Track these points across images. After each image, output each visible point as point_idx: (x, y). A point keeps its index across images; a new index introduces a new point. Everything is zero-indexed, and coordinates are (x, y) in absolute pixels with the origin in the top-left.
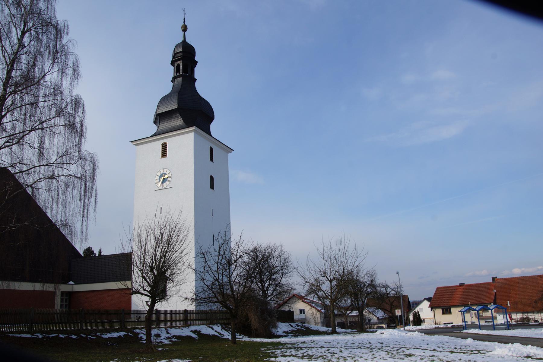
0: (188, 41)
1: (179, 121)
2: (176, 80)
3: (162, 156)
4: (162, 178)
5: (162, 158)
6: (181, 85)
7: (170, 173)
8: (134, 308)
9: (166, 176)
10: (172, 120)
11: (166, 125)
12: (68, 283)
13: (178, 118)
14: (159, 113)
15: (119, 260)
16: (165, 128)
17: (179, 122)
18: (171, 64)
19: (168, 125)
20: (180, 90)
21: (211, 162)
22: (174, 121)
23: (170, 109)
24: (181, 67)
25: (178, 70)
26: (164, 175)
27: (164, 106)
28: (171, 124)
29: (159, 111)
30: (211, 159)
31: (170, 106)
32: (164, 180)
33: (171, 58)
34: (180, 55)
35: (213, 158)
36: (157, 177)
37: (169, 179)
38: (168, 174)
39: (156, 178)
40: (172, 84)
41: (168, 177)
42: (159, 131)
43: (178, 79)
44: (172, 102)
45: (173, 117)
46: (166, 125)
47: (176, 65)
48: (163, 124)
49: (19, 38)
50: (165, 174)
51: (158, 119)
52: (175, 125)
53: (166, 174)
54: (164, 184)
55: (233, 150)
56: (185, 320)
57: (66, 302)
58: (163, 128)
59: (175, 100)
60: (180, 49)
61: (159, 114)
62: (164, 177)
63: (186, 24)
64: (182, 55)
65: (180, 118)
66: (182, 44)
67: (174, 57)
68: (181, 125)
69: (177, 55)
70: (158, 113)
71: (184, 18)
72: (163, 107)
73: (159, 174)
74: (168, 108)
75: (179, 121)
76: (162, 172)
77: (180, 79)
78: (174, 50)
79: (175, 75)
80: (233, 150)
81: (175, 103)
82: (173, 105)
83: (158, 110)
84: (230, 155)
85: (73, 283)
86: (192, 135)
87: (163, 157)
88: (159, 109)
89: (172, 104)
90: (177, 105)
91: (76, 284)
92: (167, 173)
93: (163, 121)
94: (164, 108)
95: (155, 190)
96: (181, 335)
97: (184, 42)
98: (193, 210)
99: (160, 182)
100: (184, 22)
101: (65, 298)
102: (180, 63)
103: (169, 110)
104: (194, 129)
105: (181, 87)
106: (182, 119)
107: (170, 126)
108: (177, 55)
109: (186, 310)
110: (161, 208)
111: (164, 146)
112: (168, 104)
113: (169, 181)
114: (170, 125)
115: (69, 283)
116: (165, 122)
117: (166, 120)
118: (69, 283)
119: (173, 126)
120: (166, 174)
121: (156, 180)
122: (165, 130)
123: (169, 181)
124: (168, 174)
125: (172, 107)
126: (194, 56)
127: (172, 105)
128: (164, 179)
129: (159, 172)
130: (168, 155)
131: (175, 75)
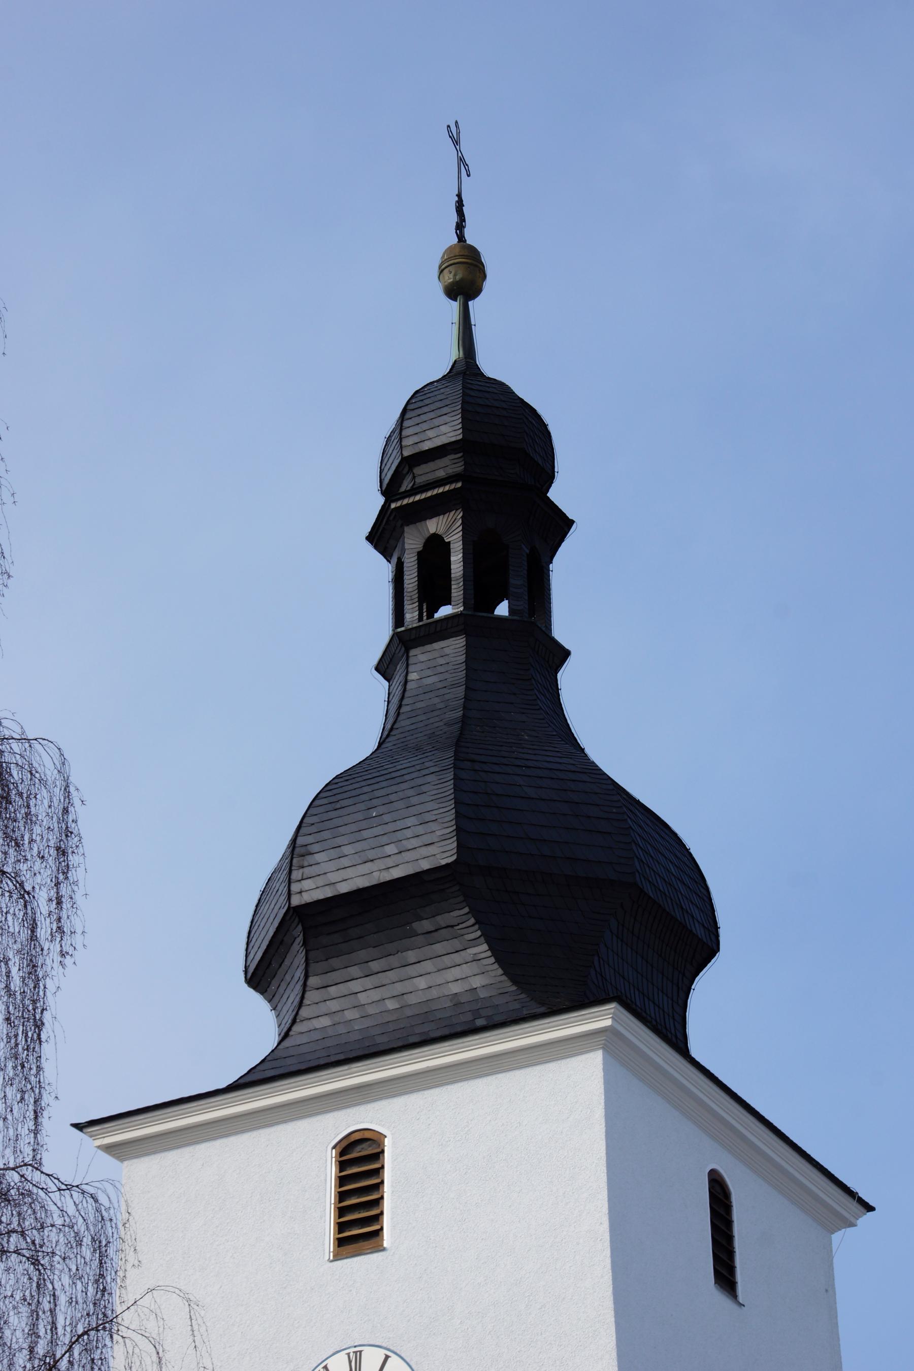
2: (419, 655)
6: (461, 691)
10: (411, 956)
13: (456, 944)
14: (307, 898)
16: (350, 1015)
17: (466, 970)
18: (370, 538)
19: (375, 995)
20: (462, 730)
22: (428, 966)
23: (397, 873)
27: (347, 850)
28: (399, 988)
29: (307, 884)
30: (724, 1256)
31: (391, 849)
34: (441, 474)
35: (731, 1269)
42: (304, 1039)
44: (410, 822)
46: (363, 998)
48: (333, 991)
49: (455, 511)
51: (297, 945)
52: (434, 993)
55: (870, 1208)
58: (337, 1018)
60: (444, 429)
61: (307, 905)
63: (470, 241)
64: (458, 468)
65: (474, 942)
66: (458, 386)
67: (390, 491)
68: (483, 994)
69: (417, 470)
70: (296, 901)
71: (459, 196)
72: (333, 853)
79: (411, 616)
80: (870, 1208)
81: (433, 826)
83: (296, 875)
88: (308, 871)
89: (408, 833)
93: (335, 962)
94: (345, 862)
100: (460, 227)
103: (387, 877)
104: (608, 1023)
105: (465, 708)
106: (491, 948)
107: (391, 1005)
108: (425, 473)
116: (354, 971)
117: (363, 954)
119: (412, 999)
122: (356, 1037)
125: (407, 856)
126: (549, 477)
127: (414, 843)
131: (411, 616)
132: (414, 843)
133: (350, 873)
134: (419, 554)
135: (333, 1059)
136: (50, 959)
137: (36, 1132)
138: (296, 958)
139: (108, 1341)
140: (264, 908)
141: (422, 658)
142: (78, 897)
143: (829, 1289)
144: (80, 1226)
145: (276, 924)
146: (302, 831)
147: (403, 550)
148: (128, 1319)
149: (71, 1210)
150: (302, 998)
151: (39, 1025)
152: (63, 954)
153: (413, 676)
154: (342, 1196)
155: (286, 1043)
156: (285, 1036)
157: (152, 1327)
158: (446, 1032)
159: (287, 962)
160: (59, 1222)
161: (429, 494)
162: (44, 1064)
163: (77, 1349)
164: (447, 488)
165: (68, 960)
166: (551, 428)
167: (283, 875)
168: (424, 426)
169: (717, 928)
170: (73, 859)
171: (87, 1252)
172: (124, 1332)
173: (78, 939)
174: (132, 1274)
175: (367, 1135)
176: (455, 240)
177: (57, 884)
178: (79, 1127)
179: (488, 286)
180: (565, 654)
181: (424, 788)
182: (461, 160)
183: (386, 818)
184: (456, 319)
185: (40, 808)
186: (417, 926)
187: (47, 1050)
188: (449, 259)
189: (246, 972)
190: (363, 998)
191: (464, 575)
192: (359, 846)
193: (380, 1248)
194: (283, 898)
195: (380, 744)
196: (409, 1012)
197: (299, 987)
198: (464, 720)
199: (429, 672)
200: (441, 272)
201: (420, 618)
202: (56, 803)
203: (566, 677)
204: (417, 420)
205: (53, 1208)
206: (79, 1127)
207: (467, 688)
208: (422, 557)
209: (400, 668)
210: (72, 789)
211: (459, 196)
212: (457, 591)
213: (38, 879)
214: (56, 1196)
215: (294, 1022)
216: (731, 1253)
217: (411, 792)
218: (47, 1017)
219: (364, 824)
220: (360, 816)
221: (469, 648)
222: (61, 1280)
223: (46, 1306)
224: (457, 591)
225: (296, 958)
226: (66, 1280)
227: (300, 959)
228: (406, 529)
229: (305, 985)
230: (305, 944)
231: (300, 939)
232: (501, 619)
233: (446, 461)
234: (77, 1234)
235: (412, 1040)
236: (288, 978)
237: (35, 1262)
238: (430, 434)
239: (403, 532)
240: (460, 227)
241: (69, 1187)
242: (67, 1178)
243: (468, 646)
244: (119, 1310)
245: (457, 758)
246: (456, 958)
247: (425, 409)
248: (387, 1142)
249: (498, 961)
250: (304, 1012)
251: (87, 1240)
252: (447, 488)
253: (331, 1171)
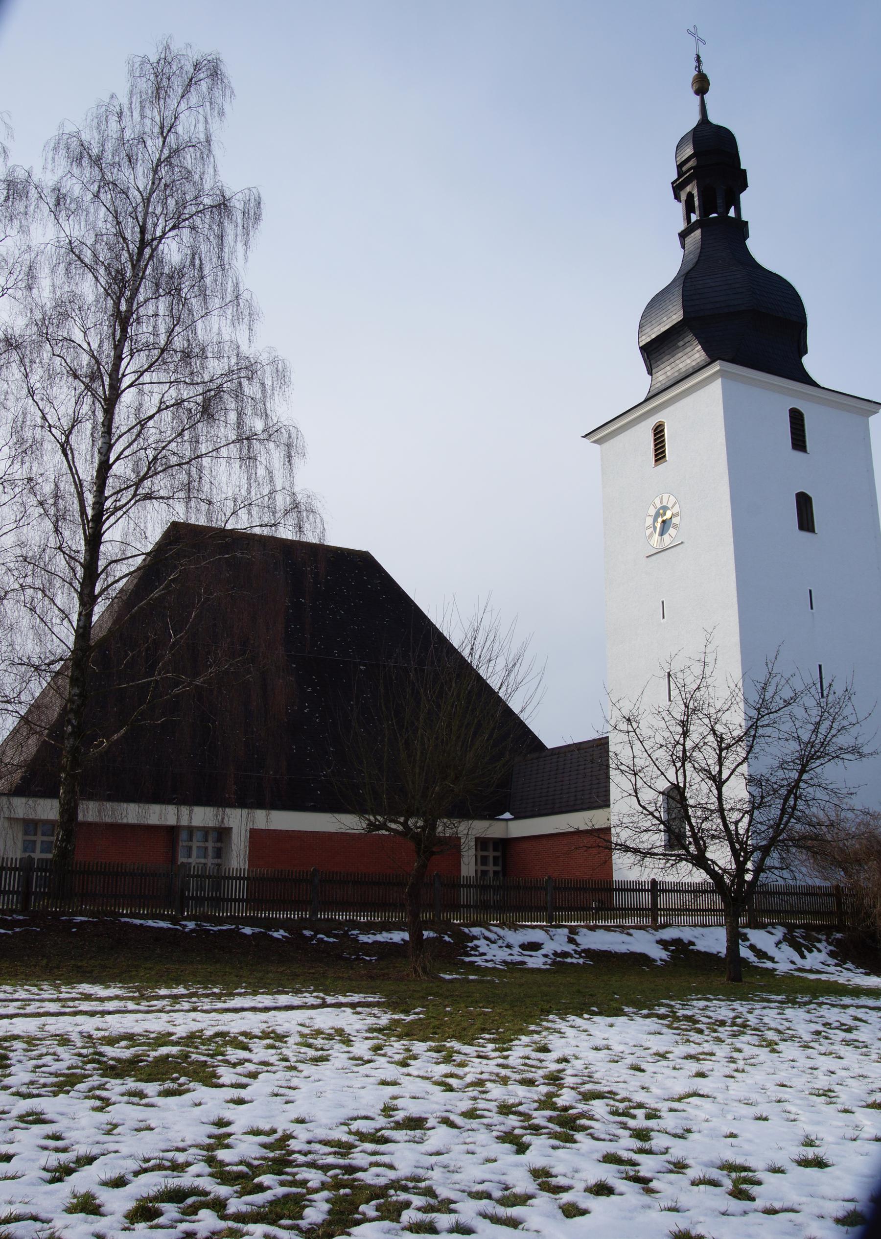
0: (715, 118)
1: (695, 354)
3: (656, 461)
4: (660, 520)
6: (699, 250)
7: (675, 503)
8: (617, 876)
9: (668, 515)
10: (680, 355)
11: (667, 371)
13: (692, 347)
21: (799, 454)
23: (667, 327)
24: (696, 199)
25: (689, 208)
36: (649, 521)
37: (675, 520)
38: (672, 508)
39: (647, 524)
43: (692, 235)
45: (679, 347)
50: (665, 508)
54: (666, 537)
56: (654, 911)
57: (495, 864)
60: (688, 150)
62: (664, 518)
73: (652, 511)
75: (695, 354)
76: (659, 506)
82: (674, 316)
87: (658, 462)
88: (643, 333)
89: (669, 311)
91: (517, 817)
92: (670, 506)
94: (653, 327)
95: (647, 557)
96: (609, 950)
97: (704, 120)
98: (735, 599)
101: (491, 854)
102: (692, 188)
104: (719, 368)
108: (684, 169)
109: (654, 882)
111: (659, 432)
113: (675, 526)
117: (666, 358)
125: (670, 320)
128: (664, 522)
129: (652, 506)
221: (703, 234)
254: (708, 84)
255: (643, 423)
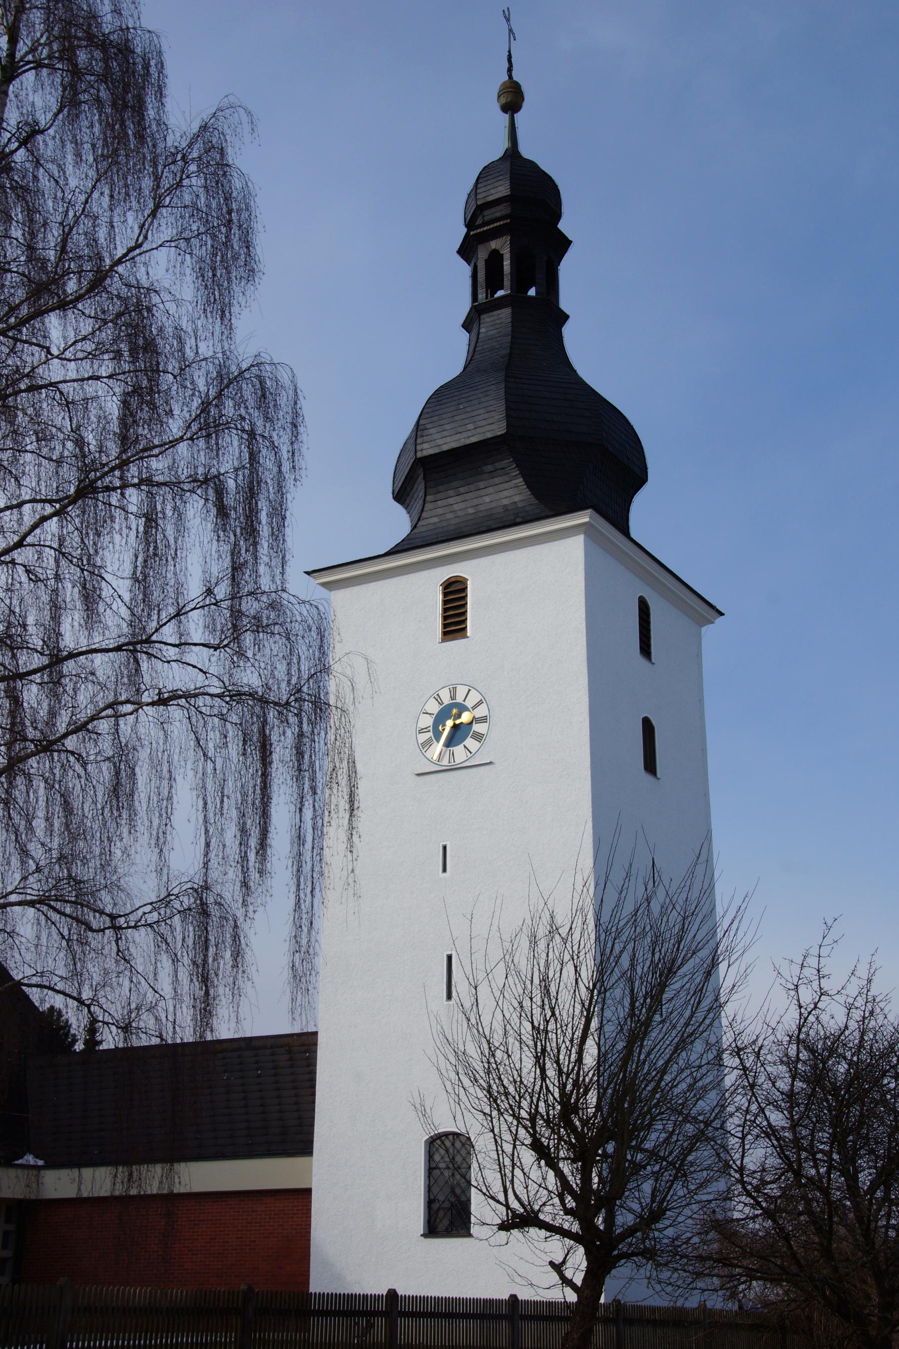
0: (526, 151)
2: (486, 318)
3: (445, 634)
4: (449, 723)
5: (443, 641)
6: (509, 339)
7: (480, 703)
9: (465, 718)
10: (482, 484)
12: (16, 1162)
13: (506, 478)
14: (425, 453)
15: (291, 1059)
16: (448, 516)
18: (459, 252)
19: (462, 506)
22: (490, 490)
23: (474, 440)
24: (507, 264)
26: (455, 711)
27: (447, 427)
28: (475, 502)
29: (425, 446)
31: (471, 426)
32: (458, 734)
33: (460, 232)
34: (498, 214)
35: (649, 646)
36: (427, 721)
37: (476, 727)
38: (474, 708)
40: (464, 337)
41: (475, 720)
44: (481, 411)
46: (456, 507)
47: (482, 254)
50: (462, 708)
52: (494, 505)
53: (466, 709)
54: (459, 750)
55: (722, 614)
59: (491, 403)
60: (500, 188)
61: (426, 457)
62: (458, 722)
63: (515, 78)
65: (515, 477)
66: (508, 164)
67: (470, 224)
69: (485, 213)
70: (419, 455)
71: (509, 52)
72: (439, 429)
73: (434, 708)
74: (465, 435)
76: (447, 700)
77: (505, 314)
78: (474, 181)
79: (481, 296)
80: (722, 614)
81: (493, 414)
83: (419, 441)
84: (710, 633)
85: (41, 1163)
86: (578, 544)
88: (425, 439)
89: (480, 418)
90: (504, 424)
91: (51, 1165)
92: (469, 703)
93: (441, 488)
94: (446, 433)
95: (418, 775)
97: (512, 154)
99: (438, 740)
100: (510, 70)
102: (503, 245)
103: (468, 442)
104: (587, 520)
105: (511, 348)
107: (471, 511)
108: (489, 214)
110: (445, 848)
112: (464, 416)
113: (478, 737)
114: (468, 504)
115: (20, 1162)
116: (451, 493)
117: (455, 484)
118: (20, 1162)
119: (482, 508)
120: (466, 709)
121: (421, 731)
123: (478, 737)
124: (474, 708)
126: (558, 216)
127: (483, 423)
128: (455, 727)
130: (472, 626)
131: (481, 296)
132: (483, 423)
133: (449, 439)
134: (486, 261)
135: (440, 539)
136: (289, 483)
137: (283, 574)
138: (420, 486)
139: (327, 678)
140: (402, 460)
141: (488, 320)
142: (304, 450)
143: (699, 655)
144: (310, 621)
145: (409, 467)
146: (423, 416)
147: (477, 259)
148: (336, 668)
149: (305, 613)
150: (423, 507)
151: (284, 518)
152: (295, 480)
153: (482, 330)
154: (445, 610)
155: (415, 531)
156: (414, 527)
157: (348, 672)
158: (501, 525)
159: (415, 488)
160: (299, 619)
161: (492, 226)
162: (286, 538)
163: (311, 681)
164: (502, 223)
165: (298, 483)
166: (560, 188)
167: (412, 441)
168: (489, 187)
169: (646, 469)
170: (301, 429)
171: (314, 634)
172: (334, 673)
173: (303, 473)
174: (338, 646)
175: (458, 579)
176: (507, 78)
177: (292, 443)
178: (308, 573)
179: (526, 105)
180: (566, 317)
181: (489, 393)
182: (511, 31)
183: (468, 409)
184: (507, 124)
185: (283, 401)
186: (484, 468)
187: (288, 531)
188: (507, 88)
189: (393, 493)
190: (456, 507)
191: (511, 273)
192: (453, 425)
193: (466, 637)
194: (413, 453)
195: (465, 368)
196: (481, 515)
197: (421, 502)
198: (511, 355)
199: (492, 328)
200: (499, 97)
201: (487, 298)
202: (290, 399)
203: (568, 331)
204: (485, 184)
205: (296, 612)
206: (308, 573)
207: (513, 337)
208: (488, 262)
209: (475, 326)
210: (298, 391)
211: (509, 52)
212: (507, 282)
213: (282, 440)
214: (297, 606)
215: (419, 519)
216: (649, 638)
217: (482, 395)
218: (288, 514)
219: (455, 413)
220: (453, 408)
221: (514, 314)
222: (302, 649)
223: (295, 661)
224: (507, 282)
225: (420, 486)
226: (304, 648)
227: (422, 485)
228: (479, 247)
229: (424, 500)
230: (424, 478)
231: (421, 476)
232: (531, 297)
233: (501, 207)
234: (308, 626)
235: (482, 529)
236: (415, 496)
237: (288, 639)
238: (493, 191)
239: (477, 249)
240: (510, 70)
241: (304, 602)
242: (303, 597)
243: (513, 313)
244: (331, 663)
245: (507, 376)
246: (505, 486)
247: (489, 177)
248: (468, 582)
249: (528, 487)
250: (424, 515)
251: (314, 628)
252: (502, 223)
253: (440, 597)
254: (523, 100)
255: (425, 574)
